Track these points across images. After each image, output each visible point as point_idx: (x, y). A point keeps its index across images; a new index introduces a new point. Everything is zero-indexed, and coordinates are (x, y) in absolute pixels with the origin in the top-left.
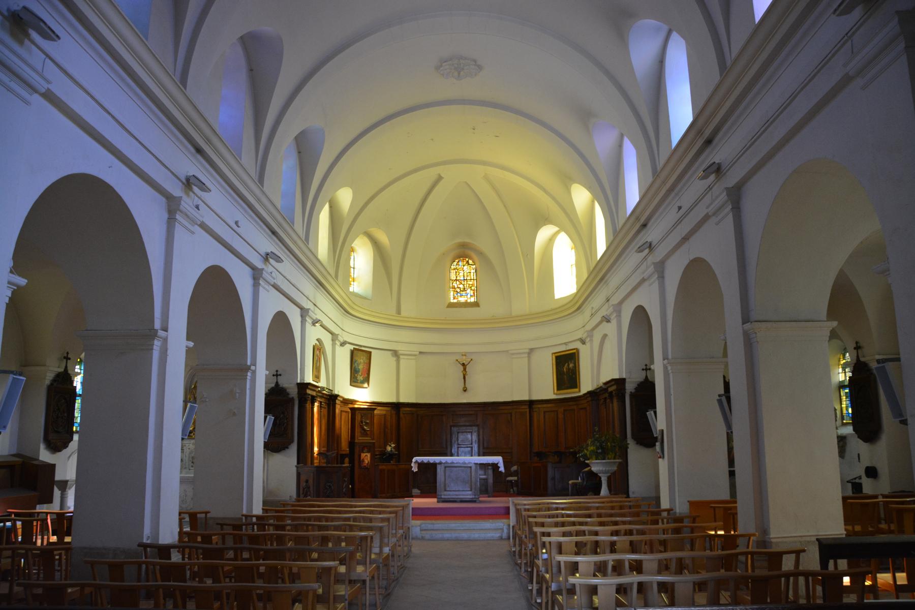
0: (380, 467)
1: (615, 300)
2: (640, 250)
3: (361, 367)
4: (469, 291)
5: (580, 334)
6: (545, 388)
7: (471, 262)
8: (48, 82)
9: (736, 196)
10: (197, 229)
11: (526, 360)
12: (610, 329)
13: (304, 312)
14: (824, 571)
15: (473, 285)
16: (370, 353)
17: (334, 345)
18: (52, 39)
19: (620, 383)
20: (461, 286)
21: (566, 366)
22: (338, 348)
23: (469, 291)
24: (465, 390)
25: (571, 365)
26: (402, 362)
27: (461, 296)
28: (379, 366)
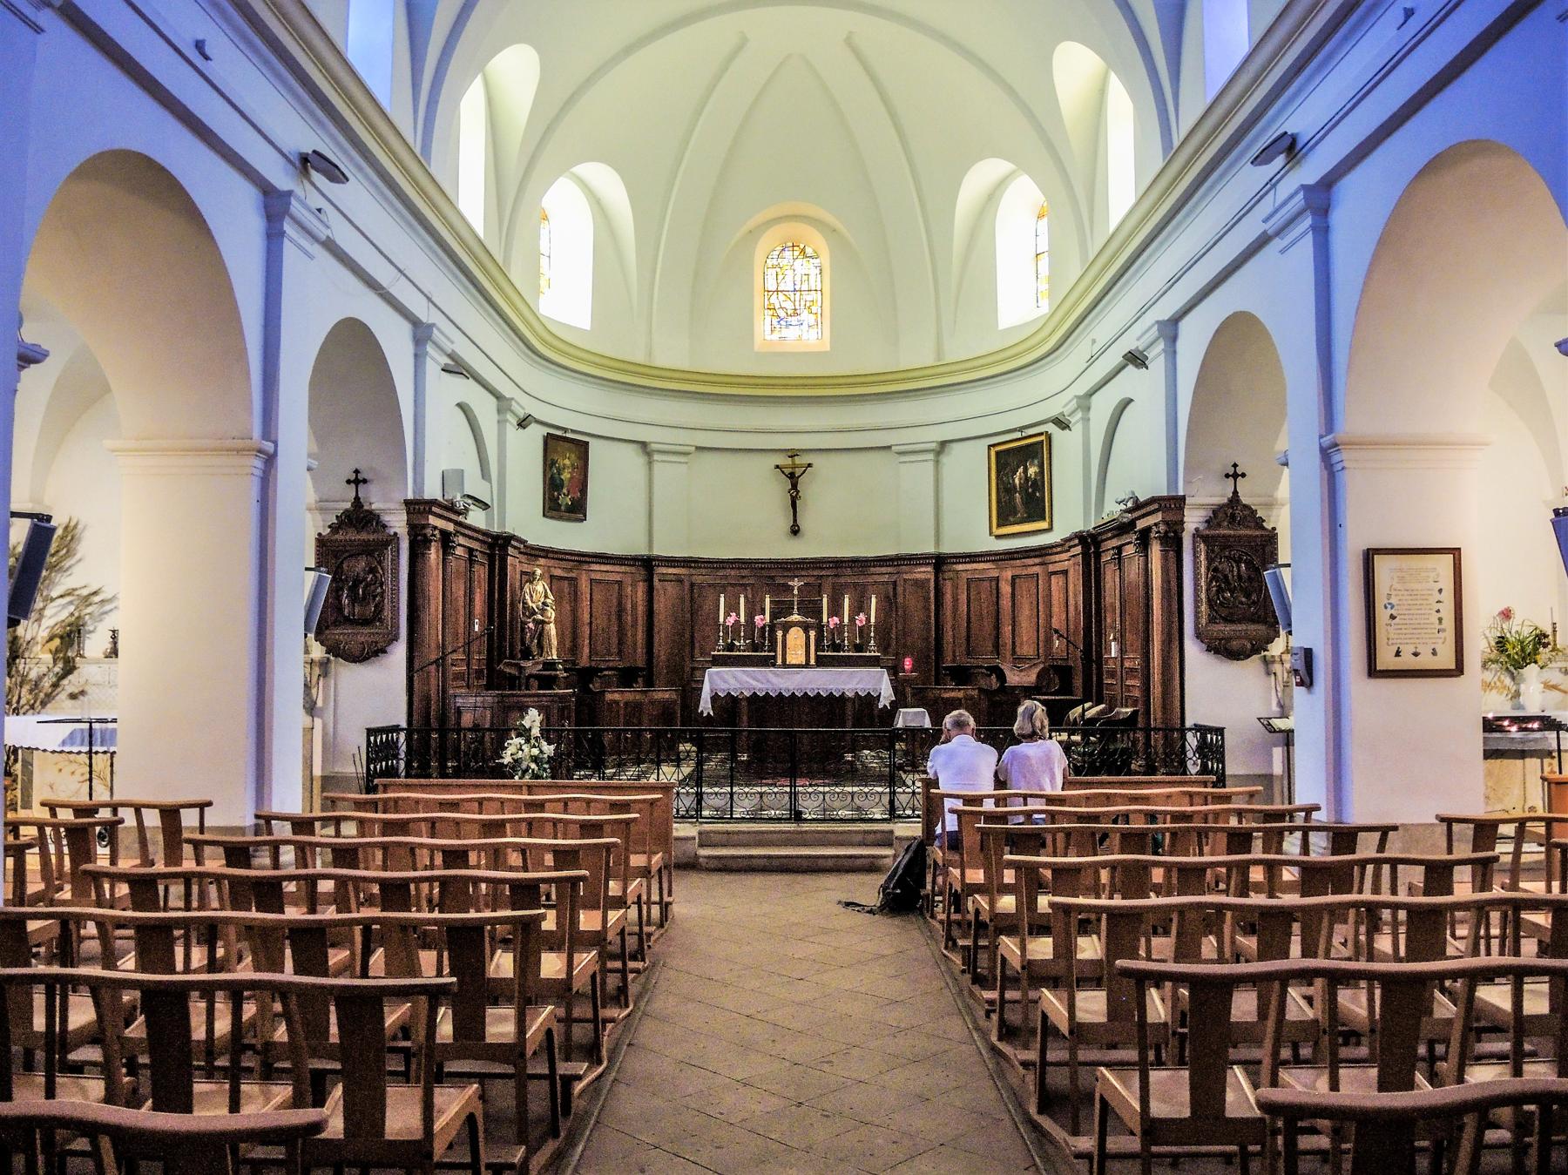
0: (609, 697)
1: (1165, 310)
2: (1262, 159)
4: (805, 315)
5: (1053, 409)
7: (809, 251)
9: (1320, 200)
10: (316, 249)
11: (931, 465)
12: (1144, 385)
13: (421, 334)
14: (1305, 858)
17: (419, 358)
18: (339, 181)
19: (1173, 505)
20: (789, 305)
21: (1020, 478)
22: (512, 431)
23: (805, 315)
24: (795, 531)
25: (1032, 471)
26: (656, 466)
27: (788, 325)
28: (611, 475)
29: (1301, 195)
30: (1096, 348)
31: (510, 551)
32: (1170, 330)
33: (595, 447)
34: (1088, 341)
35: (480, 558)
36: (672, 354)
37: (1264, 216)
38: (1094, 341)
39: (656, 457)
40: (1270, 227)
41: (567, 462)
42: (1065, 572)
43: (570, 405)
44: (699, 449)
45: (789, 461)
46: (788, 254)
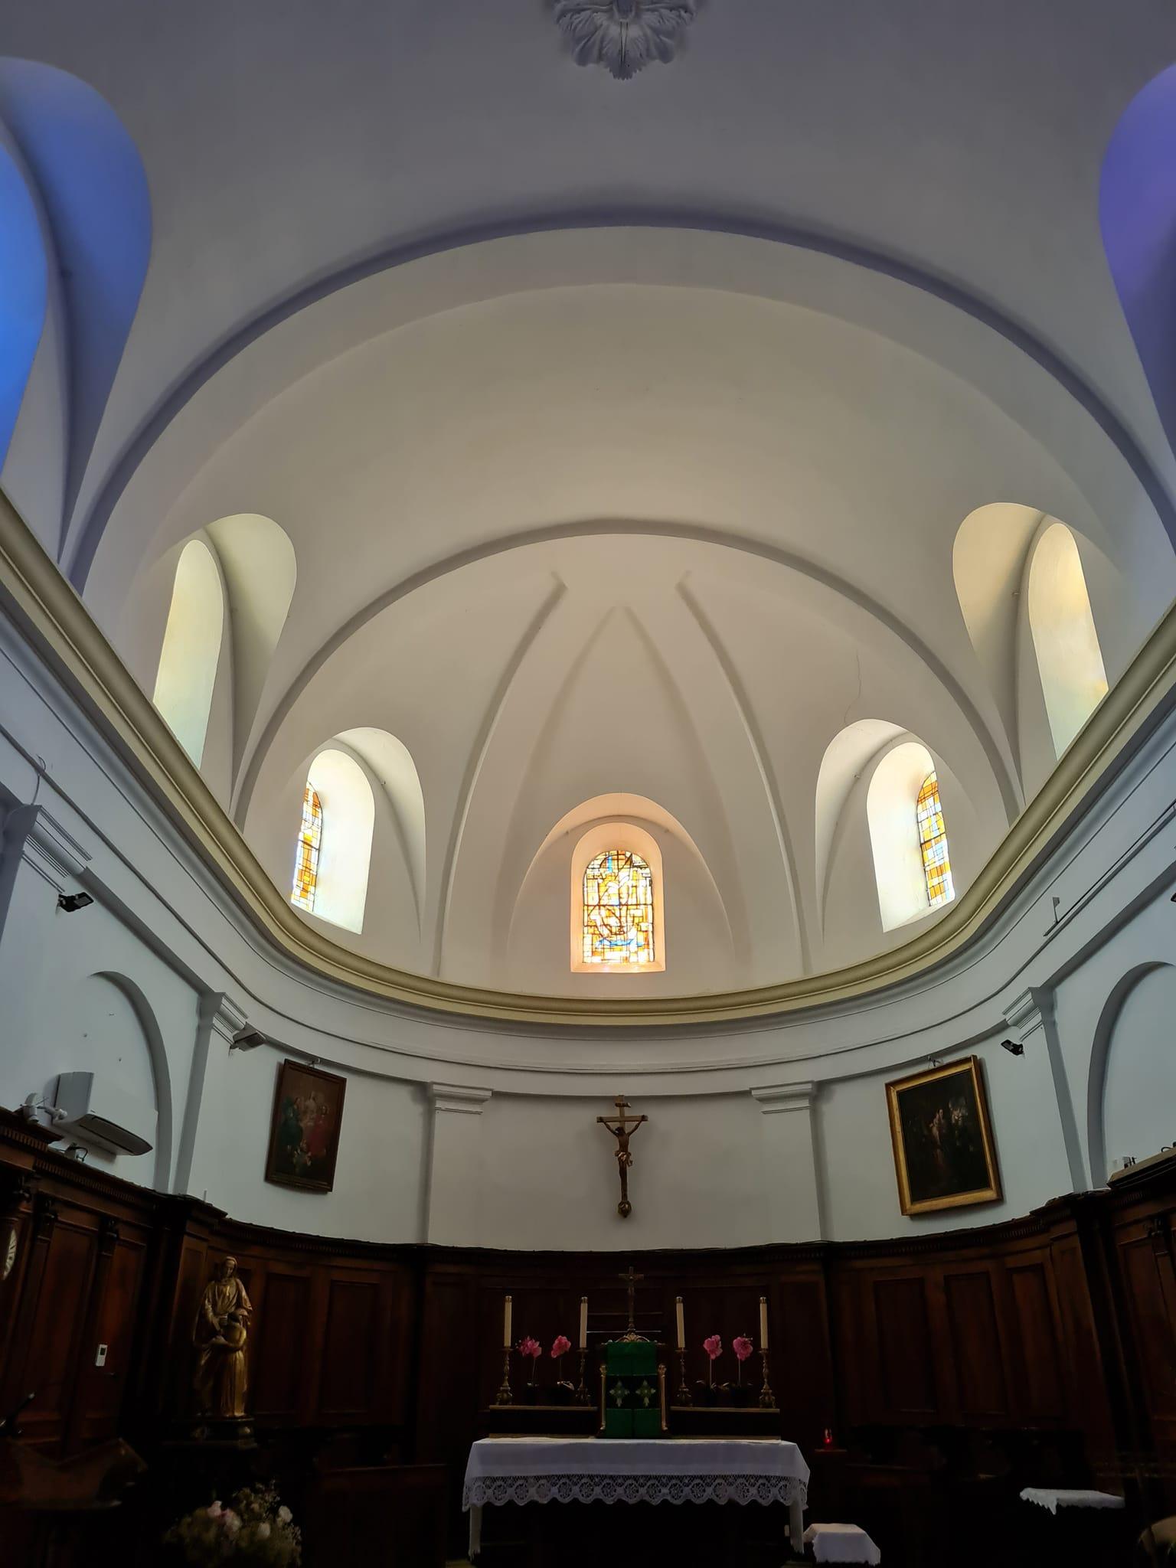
1: (1039, 975)
3: (307, 1123)
4: (632, 933)
6: (869, 1200)
7: (637, 860)
8: (88, 858)
15: (644, 918)
16: (344, 1081)
20: (613, 921)
21: (942, 1125)
23: (632, 933)
24: (625, 1211)
25: (957, 1115)
26: (439, 1118)
27: (612, 946)
28: (370, 1127)
29: (1029, 996)
30: (1062, 910)
31: (190, 1227)
32: (1045, 998)
33: (356, 1093)
34: (1046, 901)
35: (125, 1234)
36: (467, 967)
37: (1004, 1009)
38: (1056, 901)
39: (439, 1104)
40: (1010, 1017)
41: (311, 1103)
42: (1038, 1269)
43: (322, 1027)
44: (498, 1095)
45: (616, 1112)
46: (612, 864)
